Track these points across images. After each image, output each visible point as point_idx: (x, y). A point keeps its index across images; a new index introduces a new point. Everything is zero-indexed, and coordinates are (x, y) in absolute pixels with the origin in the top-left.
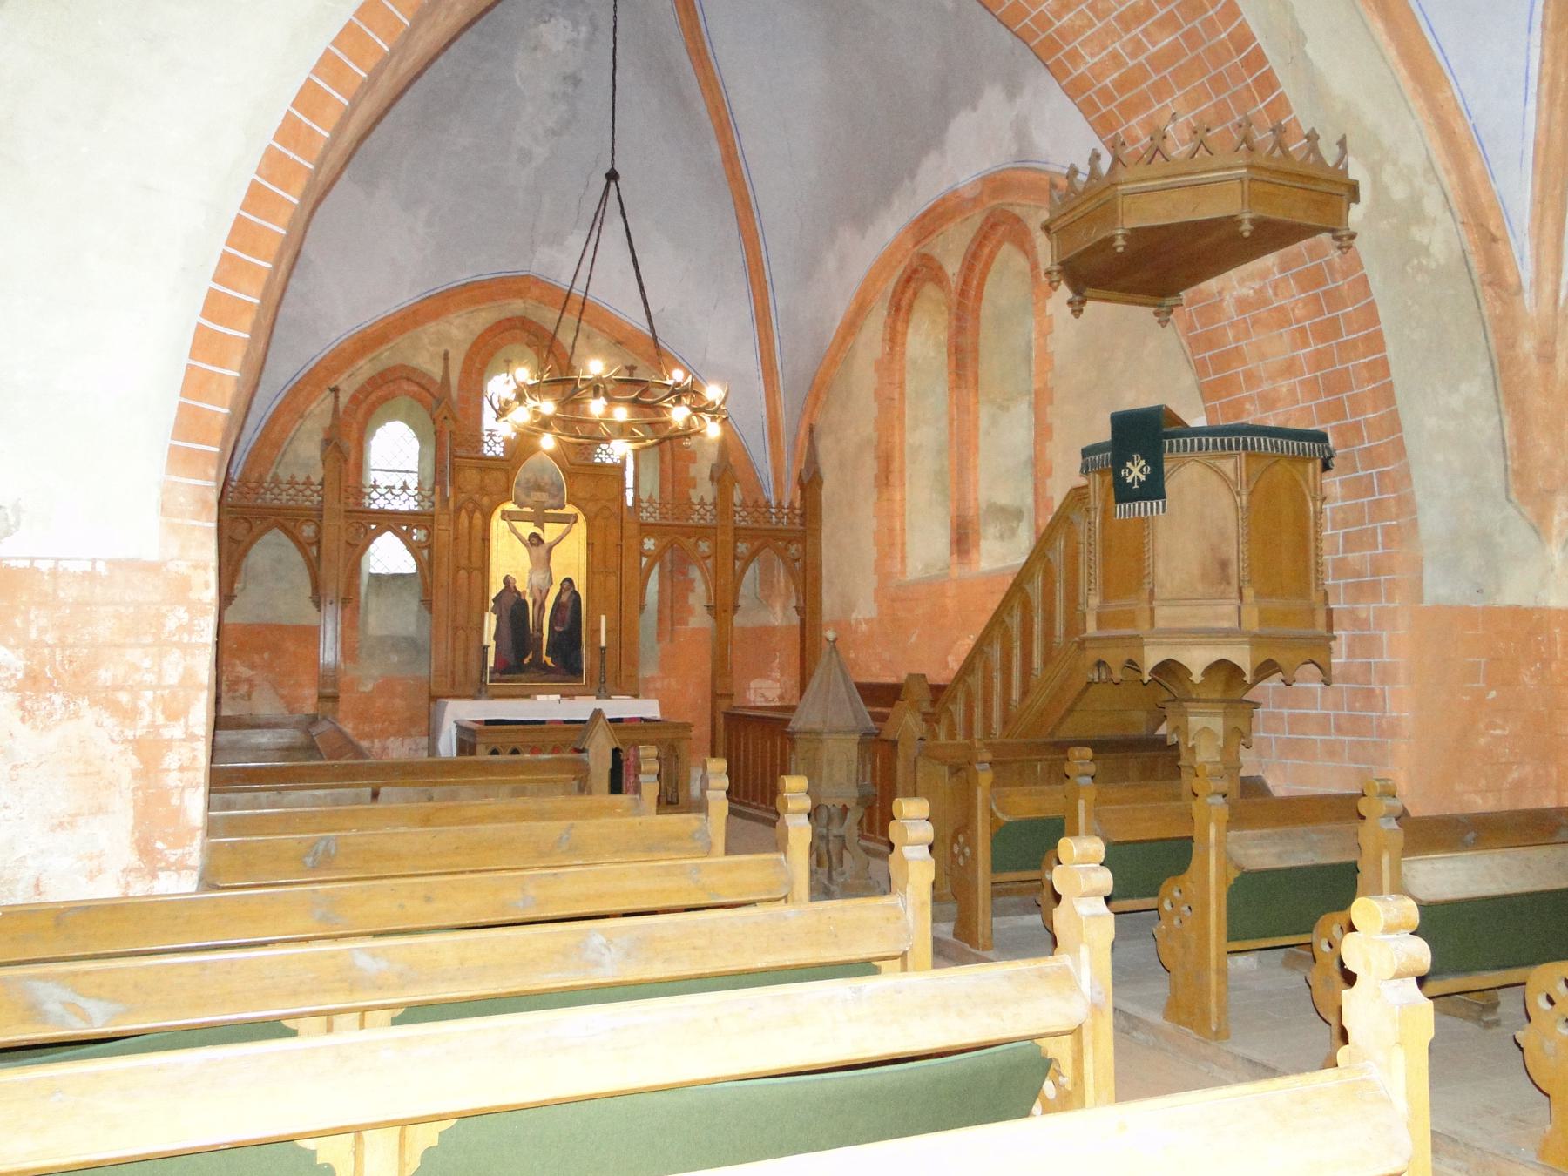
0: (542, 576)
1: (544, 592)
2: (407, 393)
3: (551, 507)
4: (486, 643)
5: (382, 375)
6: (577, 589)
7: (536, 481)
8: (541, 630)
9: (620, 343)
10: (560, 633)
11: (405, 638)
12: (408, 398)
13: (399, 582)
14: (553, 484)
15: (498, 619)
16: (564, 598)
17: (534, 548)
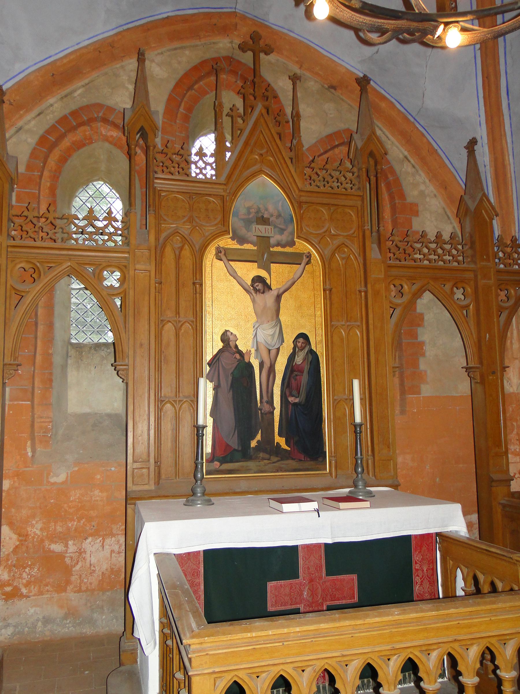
0: (271, 332)
1: (273, 352)
2: (106, 139)
3: (278, 244)
4: (201, 422)
5: (74, 113)
6: (313, 348)
7: (258, 211)
8: (271, 402)
9: (333, 87)
10: (295, 404)
11: (109, 416)
12: (107, 145)
13: (103, 353)
14: (279, 216)
15: (216, 389)
16: (299, 360)
17: (259, 297)
